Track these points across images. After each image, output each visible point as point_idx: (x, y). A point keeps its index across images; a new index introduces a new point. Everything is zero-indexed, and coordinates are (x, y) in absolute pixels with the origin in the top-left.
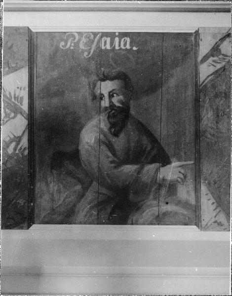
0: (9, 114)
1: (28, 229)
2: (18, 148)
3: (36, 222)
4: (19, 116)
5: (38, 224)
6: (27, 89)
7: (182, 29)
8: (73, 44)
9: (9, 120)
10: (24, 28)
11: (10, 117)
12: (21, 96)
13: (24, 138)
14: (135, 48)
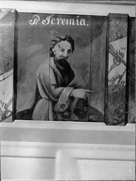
0: (116, 63)
1: (125, 126)
2: (121, 82)
3: (128, 122)
4: (122, 64)
5: (129, 123)
6: (126, 49)
7: (59, 12)
8: (37, 22)
9: (116, 66)
10: (125, 15)
11: (117, 64)
12: (123, 53)
13: (52, 77)
14: (87, 25)
